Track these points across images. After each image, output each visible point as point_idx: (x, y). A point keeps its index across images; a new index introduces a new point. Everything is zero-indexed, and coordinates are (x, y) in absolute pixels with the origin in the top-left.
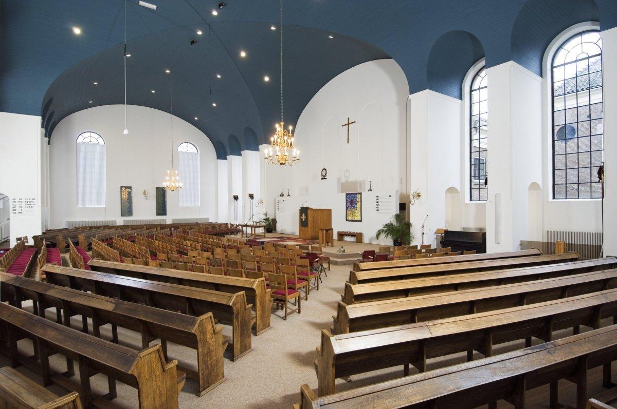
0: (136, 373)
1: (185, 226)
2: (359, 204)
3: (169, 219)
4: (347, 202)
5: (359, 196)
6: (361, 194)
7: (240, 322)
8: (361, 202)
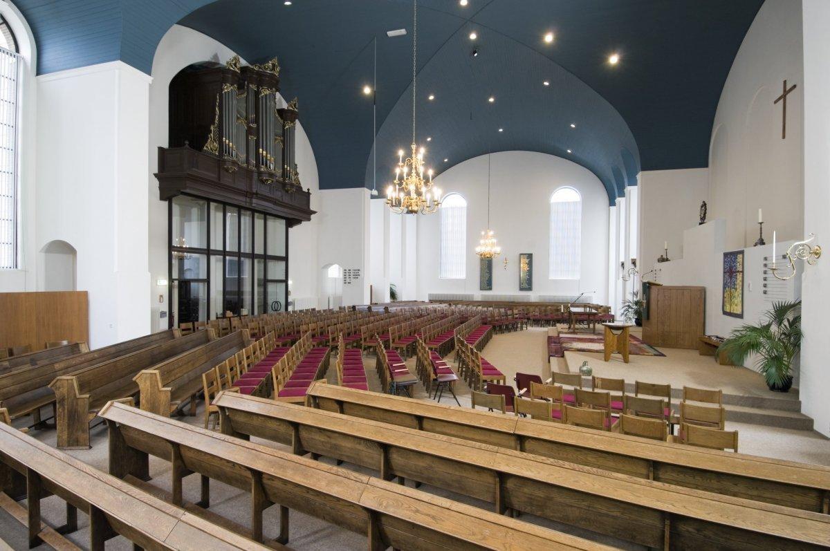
0: (169, 475)
1: (537, 306)
2: (739, 277)
3: (533, 296)
4: (724, 272)
5: (740, 256)
6: (742, 252)
7: (66, 411)
8: (743, 272)
